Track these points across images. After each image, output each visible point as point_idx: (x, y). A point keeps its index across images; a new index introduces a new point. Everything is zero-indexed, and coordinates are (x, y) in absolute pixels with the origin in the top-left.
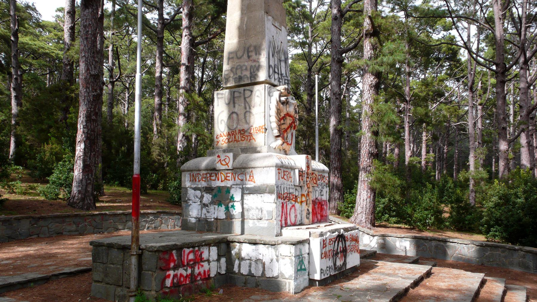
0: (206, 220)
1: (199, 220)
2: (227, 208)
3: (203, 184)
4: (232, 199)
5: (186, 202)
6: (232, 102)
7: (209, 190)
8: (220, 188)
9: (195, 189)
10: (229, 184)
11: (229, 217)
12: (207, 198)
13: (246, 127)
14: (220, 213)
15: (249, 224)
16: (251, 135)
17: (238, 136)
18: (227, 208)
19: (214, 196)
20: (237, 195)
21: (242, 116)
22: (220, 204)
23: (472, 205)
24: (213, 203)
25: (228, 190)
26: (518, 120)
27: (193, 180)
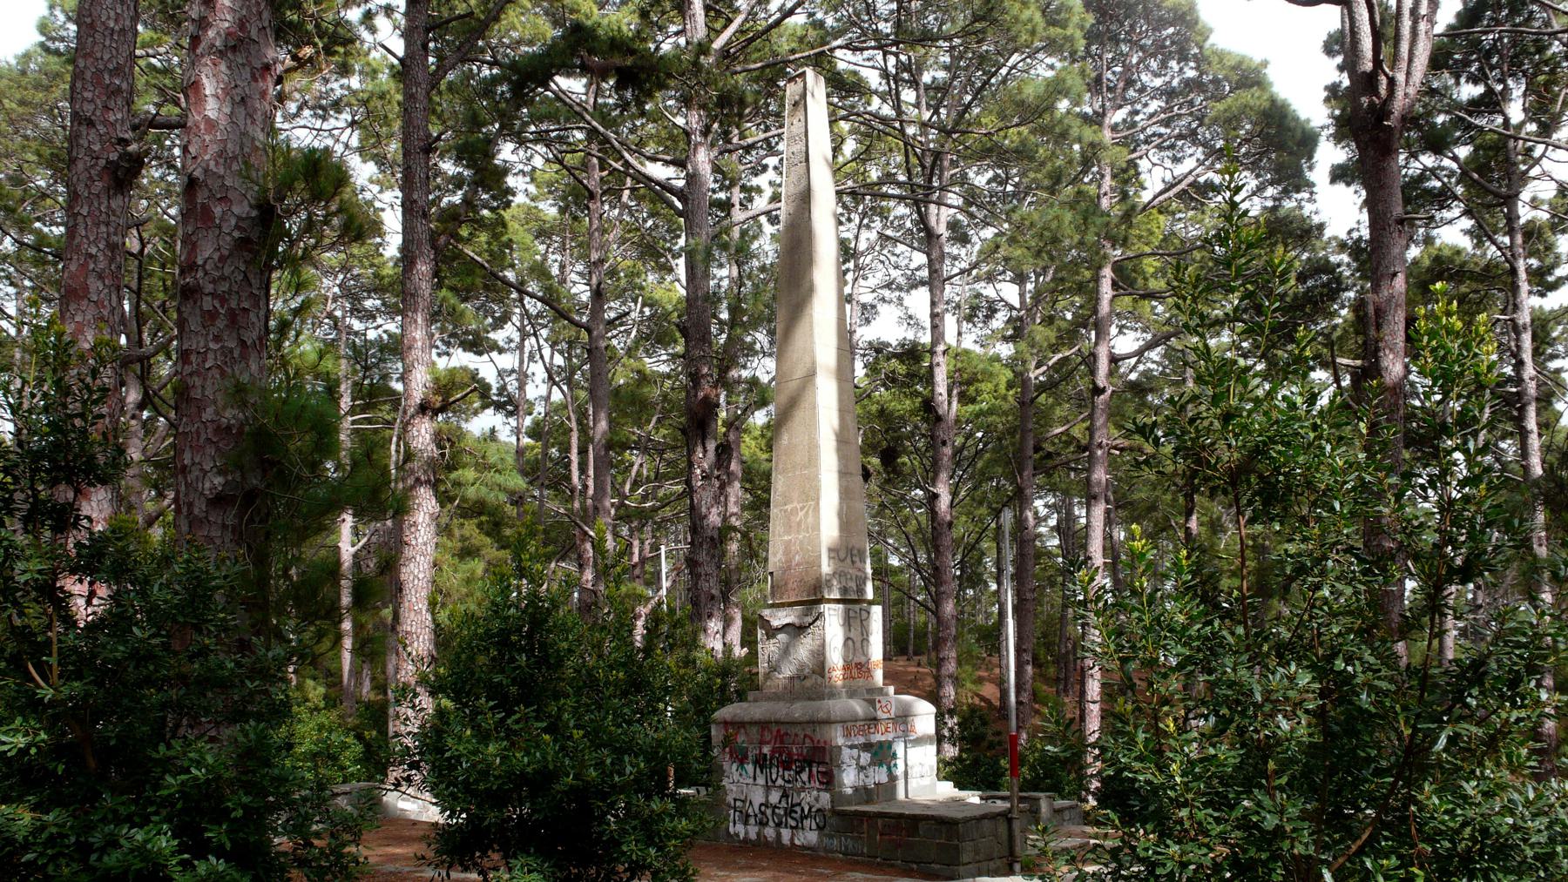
0: (865, 788)
1: (856, 789)
2: (889, 769)
3: (862, 740)
4: (894, 756)
5: (839, 766)
6: (848, 622)
7: (867, 747)
8: (880, 743)
9: (851, 747)
10: (890, 737)
11: (893, 778)
12: (865, 758)
13: (863, 659)
14: (881, 775)
15: (913, 784)
16: (869, 671)
17: (855, 671)
18: (889, 769)
19: (874, 755)
20: (899, 748)
21: (858, 645)
22: (880, 765)
23: (742, 836)
24: (872, 763)
25: (890, 744)
26: (763, 269)
27: (847, 735)
